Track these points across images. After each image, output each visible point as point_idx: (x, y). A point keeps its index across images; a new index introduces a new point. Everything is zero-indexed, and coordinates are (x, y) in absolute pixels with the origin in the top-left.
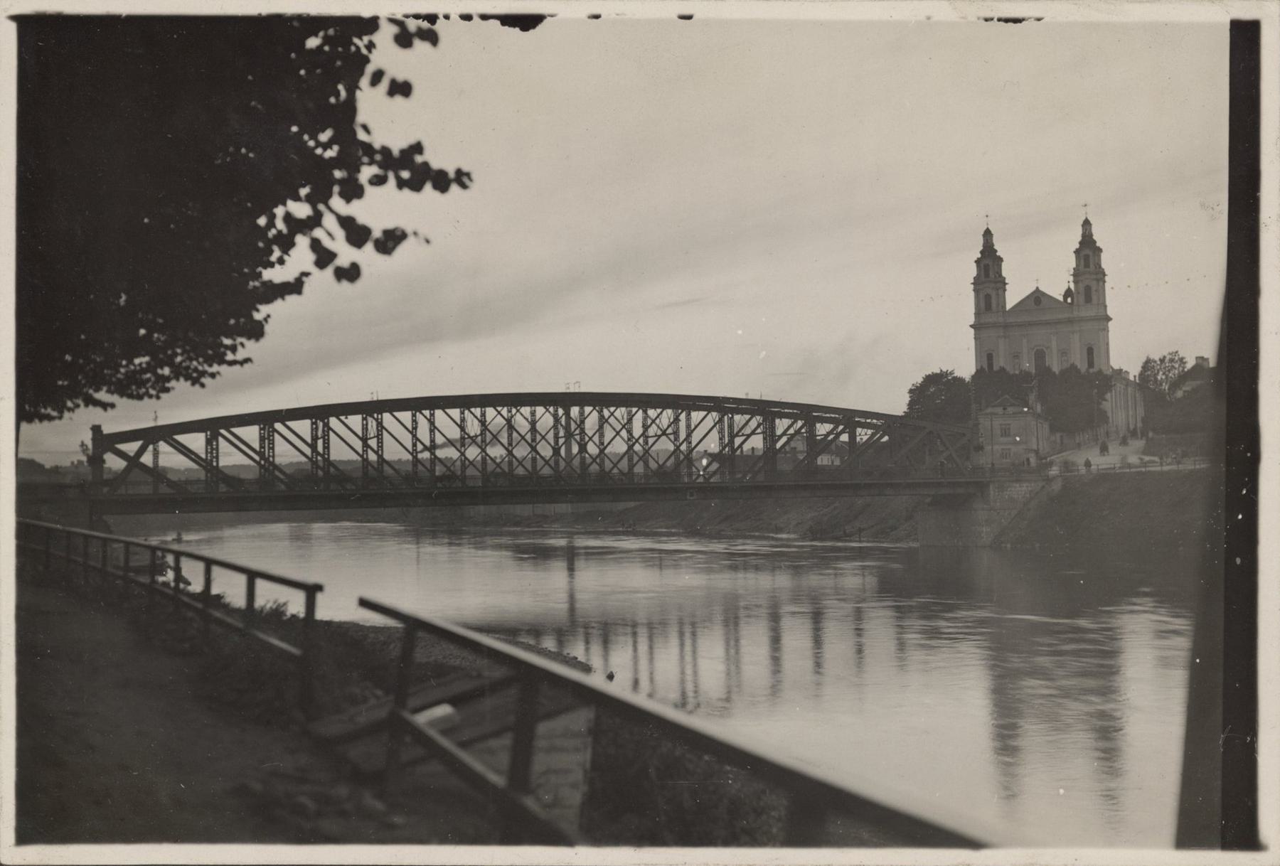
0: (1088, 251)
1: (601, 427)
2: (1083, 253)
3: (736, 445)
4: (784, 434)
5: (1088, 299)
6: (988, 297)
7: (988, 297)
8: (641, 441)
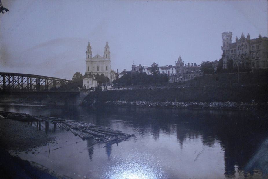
0: (107, 47)
1: (13, 80)
2: (106, 48)
3: (40, 84)
4: (43, 82)
5: (107, 57)
6: (89, 55)
7: (89, 55)
8: (10, 82)
